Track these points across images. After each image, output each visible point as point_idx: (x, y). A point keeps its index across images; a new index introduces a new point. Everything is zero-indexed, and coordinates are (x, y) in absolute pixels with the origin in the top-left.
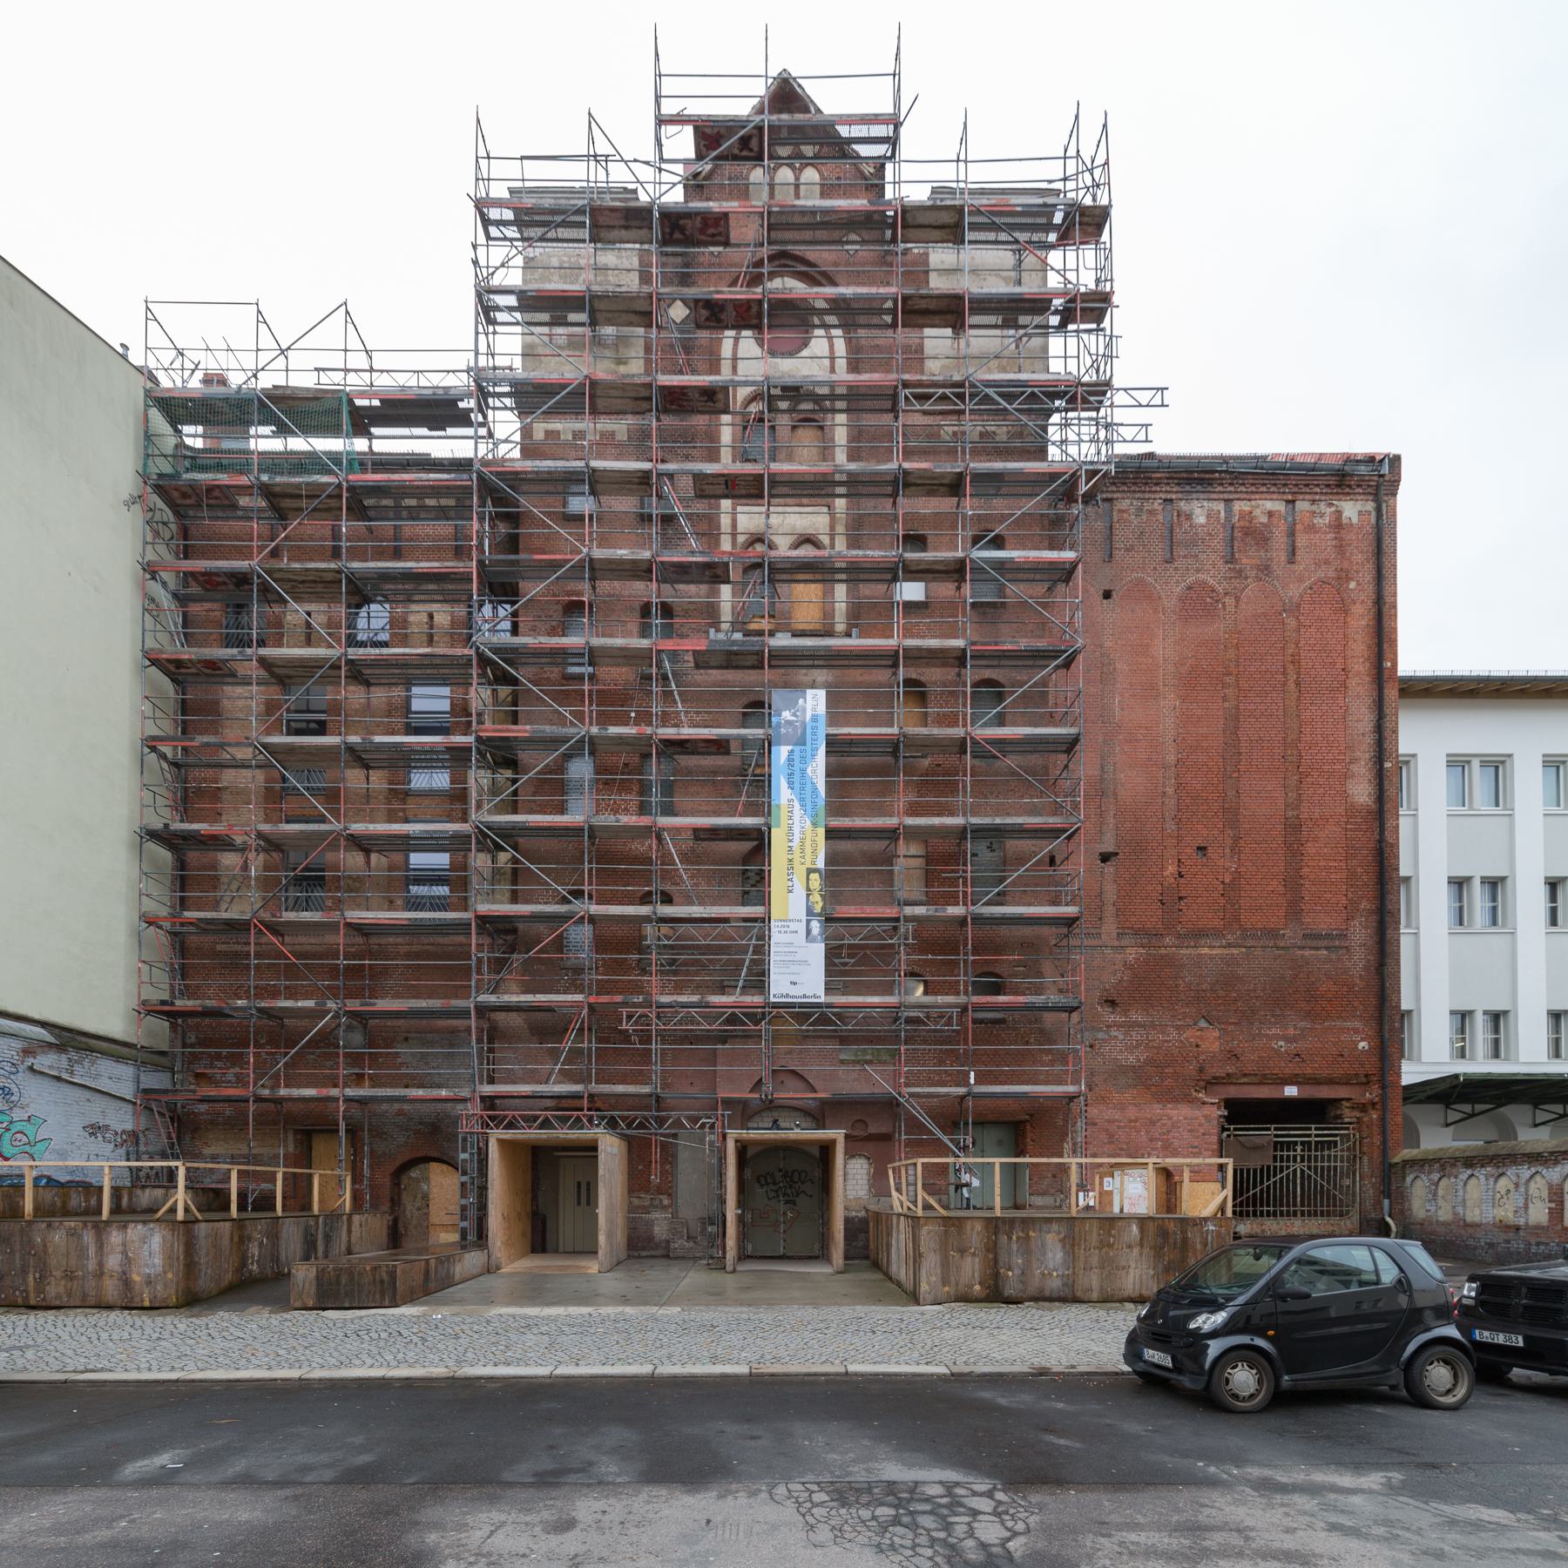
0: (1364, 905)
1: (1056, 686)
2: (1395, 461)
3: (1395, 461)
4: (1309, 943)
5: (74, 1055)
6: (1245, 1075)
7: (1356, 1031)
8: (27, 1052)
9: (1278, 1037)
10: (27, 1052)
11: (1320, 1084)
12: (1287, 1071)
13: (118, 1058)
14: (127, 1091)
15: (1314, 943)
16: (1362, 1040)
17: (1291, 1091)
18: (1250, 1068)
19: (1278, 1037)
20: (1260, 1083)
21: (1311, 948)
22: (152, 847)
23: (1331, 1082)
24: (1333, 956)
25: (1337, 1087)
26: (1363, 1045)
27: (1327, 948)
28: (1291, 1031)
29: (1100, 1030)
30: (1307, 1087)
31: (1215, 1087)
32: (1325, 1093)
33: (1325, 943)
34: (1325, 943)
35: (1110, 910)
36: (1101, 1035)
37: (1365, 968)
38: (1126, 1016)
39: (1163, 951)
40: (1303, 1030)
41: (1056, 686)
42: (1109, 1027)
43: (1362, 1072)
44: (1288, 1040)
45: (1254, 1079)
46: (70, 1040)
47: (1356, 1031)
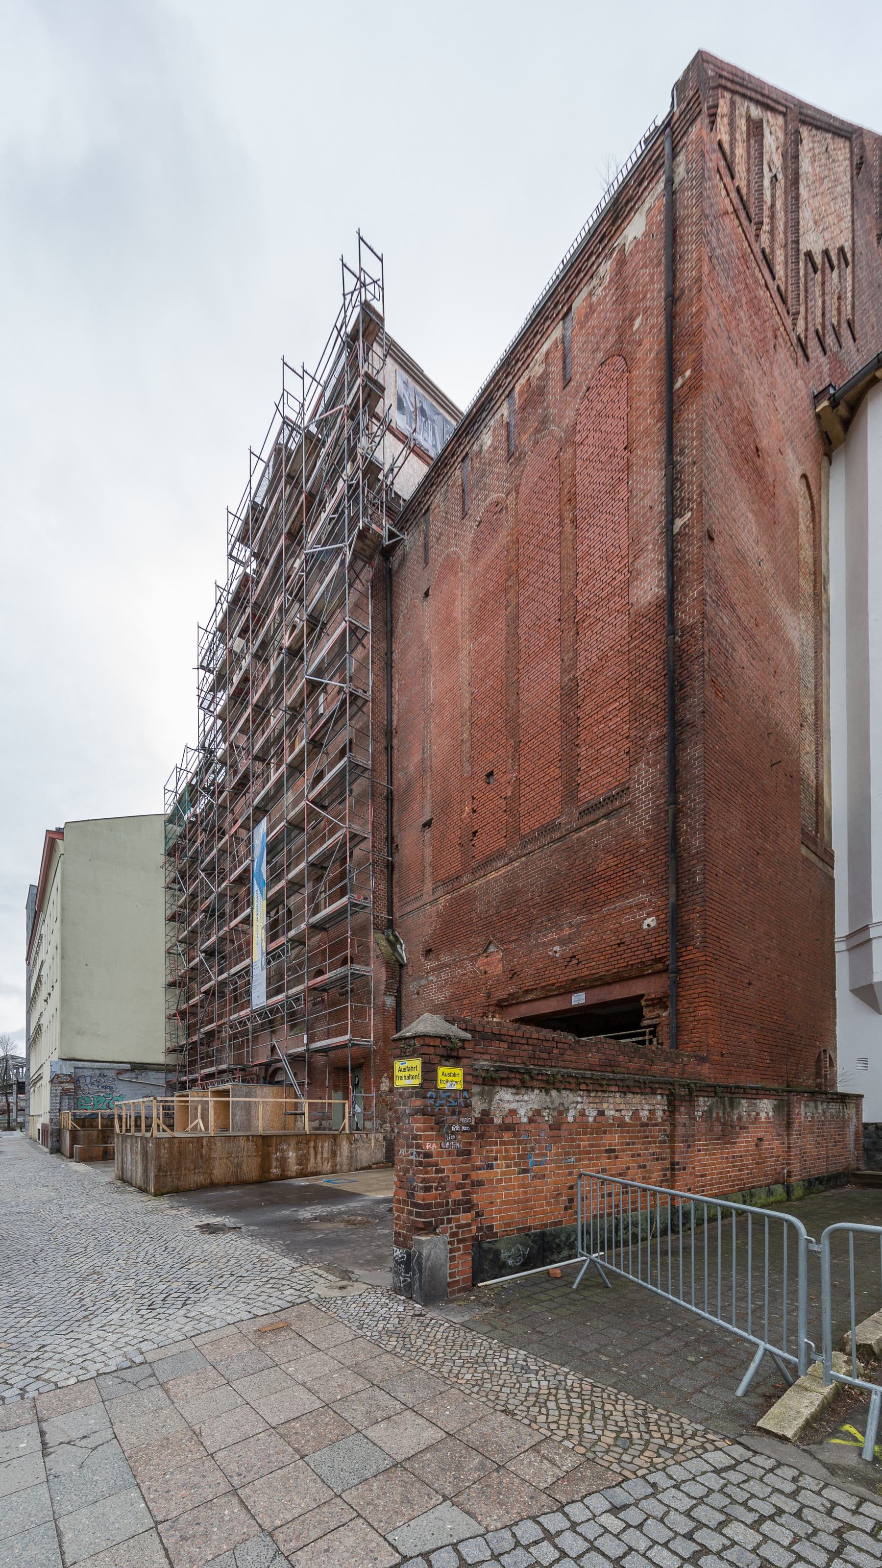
0: (654, 733)
1: (341, 689)
2: (701, 59)
3: (701, 59)
4: (587, 819)
5: (137, 1072)
6: (527, 992)
7: (641, 906)
8: (118, 1074)
9: (553, 942)
10: (118, 1074)
11: (609, 984)
12: (563, 978)
13: (158, 1071)
14: (163, 1083)
15: (591, 817)
16: (649, 915)
17: (579, 999)
18: (529, 983)
19: (553, 942)
20: (546, 997)
21: (588, 825)
22: (172, 989)
23: (619, 979)
24: (613, 822)
25: (630, 983)
26: (651, 922)
27: (606, 816)
28: (567, 932)
29: (422, 977)
30: (596, 991)
31: (510, 1009)
32: (618, 992)
33: (603, 811)
34: (603, 811)
35: (428, 870)
36: (423, 982)
37: (654, 819)
38: (438, 960)
39: (462, 891)
40: (578, 925)
41: (341, 689)
42: (427, 973)
43: (648, 957)
44: (562, 942)
45: (539, 994)
46: (138, 1067)
47: (641, 906)
